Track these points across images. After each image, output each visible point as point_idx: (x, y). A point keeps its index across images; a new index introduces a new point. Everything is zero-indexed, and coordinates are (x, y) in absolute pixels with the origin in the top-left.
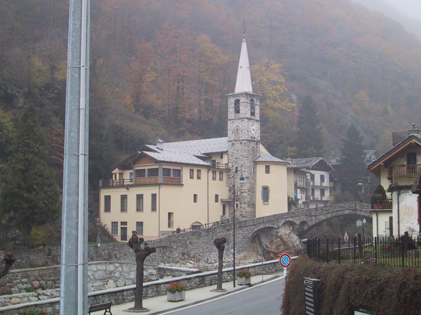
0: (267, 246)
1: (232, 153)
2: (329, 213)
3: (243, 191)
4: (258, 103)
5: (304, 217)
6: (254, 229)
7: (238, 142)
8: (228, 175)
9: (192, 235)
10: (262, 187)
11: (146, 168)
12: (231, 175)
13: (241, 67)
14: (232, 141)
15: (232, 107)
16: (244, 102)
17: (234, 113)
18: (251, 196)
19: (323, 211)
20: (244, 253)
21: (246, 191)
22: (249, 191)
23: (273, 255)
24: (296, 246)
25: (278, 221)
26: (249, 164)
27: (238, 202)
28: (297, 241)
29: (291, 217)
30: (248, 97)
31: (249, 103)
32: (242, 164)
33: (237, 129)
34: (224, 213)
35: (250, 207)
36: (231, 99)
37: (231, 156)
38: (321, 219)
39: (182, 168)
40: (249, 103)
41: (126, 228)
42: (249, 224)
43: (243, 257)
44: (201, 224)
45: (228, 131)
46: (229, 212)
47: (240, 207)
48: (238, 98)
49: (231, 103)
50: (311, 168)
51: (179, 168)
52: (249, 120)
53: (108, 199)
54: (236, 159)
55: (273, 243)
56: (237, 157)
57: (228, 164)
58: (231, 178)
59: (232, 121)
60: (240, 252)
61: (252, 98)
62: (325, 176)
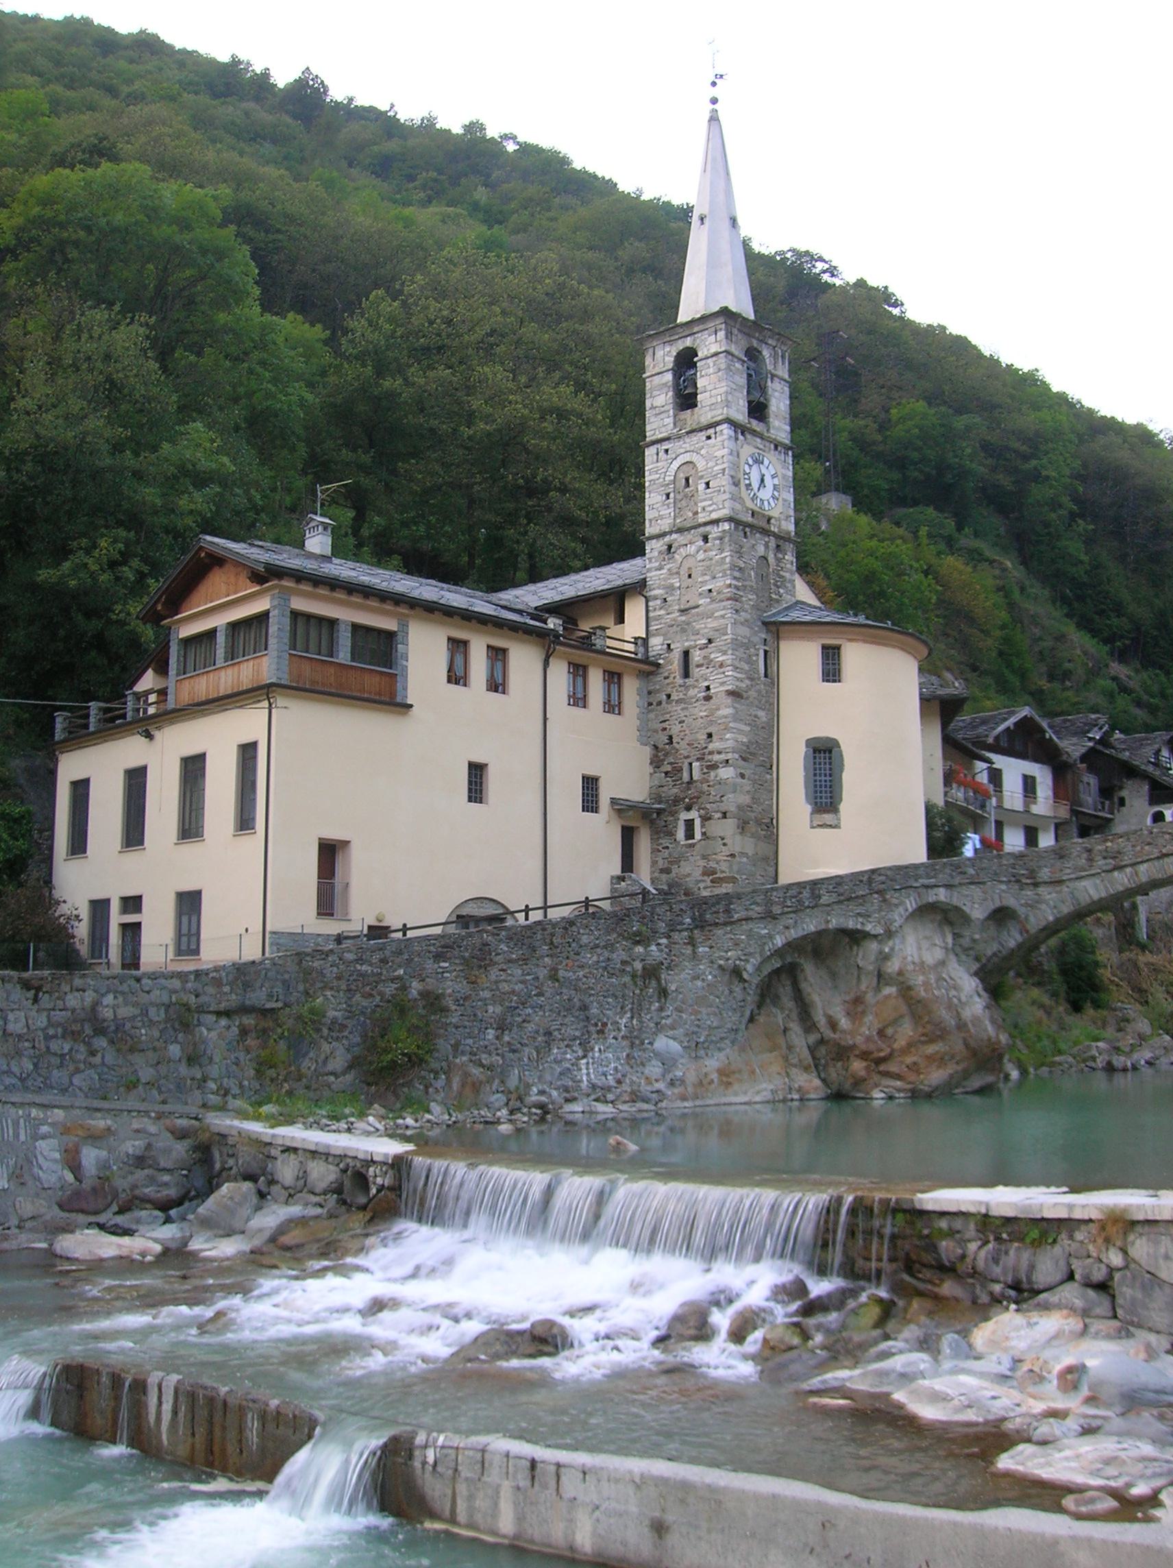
0: (833, 1025)
1: (665, 587)
2: (1120, 868)
3: (716, 757)
4: (783, 371)
5: (1004, 887)
6: (771, 937)
7: (688, 536)
8: (649, 693)
9: (438, 957)
10: (809, 742)
11: (220, 621)
12: (658, 691)
13: (702, 219)
14: (663, 535)
15: (665, 384)
16: (716, 354)
17: (671, 412)
18: (754, 782)
19: (1090, 860)
20: (722, 1055)
21: (729, 756)
22: (744, 759)
23: (864, 1064)
24: (970, 1025)
25: (885, 900)
26: (744, 631)
27: (693, 814)
28: (977, 999)
29: (948, 886)
30: (735, 331)
31: (740, 359)
32: (711, 635)
33: (687, 480)
34: (628, 862)
35: (753, 836)
36: (660, 353)
37: (658, 602)
38: (1084, 900)
39: (404, 626)
40: (740, 359)
41: (139, 924)
42: (743, 914)
43: (714, 1076)
44: (503, 906)
45: (647, 495)
46: (654, 863)
47: (704, 834)
48: (688, 342)
49: (657, 370)
50: (990, 740)
51: (389, 624)
52: (743, 434)
53: (81, 789)
54: (682, 611)
55: (860, 1009)
56: (688, 606)
57: (645, 641)
58: (660, 703)
59: (666, 446)
60: (702, 1053)
61: (755, 343)
62: (1038, 780)
